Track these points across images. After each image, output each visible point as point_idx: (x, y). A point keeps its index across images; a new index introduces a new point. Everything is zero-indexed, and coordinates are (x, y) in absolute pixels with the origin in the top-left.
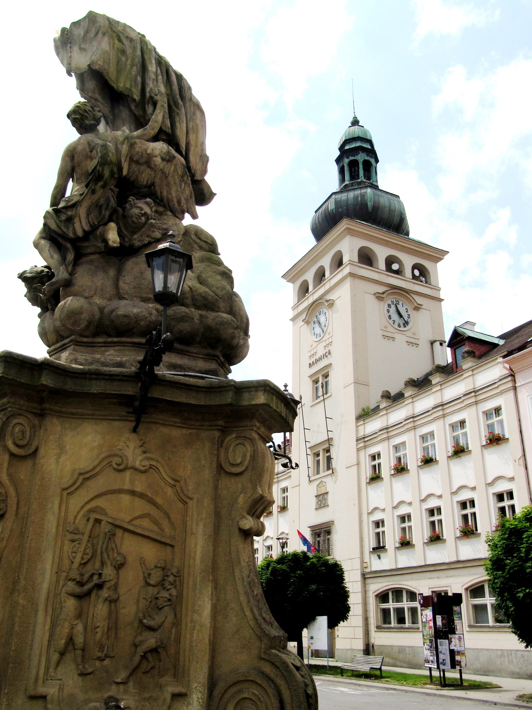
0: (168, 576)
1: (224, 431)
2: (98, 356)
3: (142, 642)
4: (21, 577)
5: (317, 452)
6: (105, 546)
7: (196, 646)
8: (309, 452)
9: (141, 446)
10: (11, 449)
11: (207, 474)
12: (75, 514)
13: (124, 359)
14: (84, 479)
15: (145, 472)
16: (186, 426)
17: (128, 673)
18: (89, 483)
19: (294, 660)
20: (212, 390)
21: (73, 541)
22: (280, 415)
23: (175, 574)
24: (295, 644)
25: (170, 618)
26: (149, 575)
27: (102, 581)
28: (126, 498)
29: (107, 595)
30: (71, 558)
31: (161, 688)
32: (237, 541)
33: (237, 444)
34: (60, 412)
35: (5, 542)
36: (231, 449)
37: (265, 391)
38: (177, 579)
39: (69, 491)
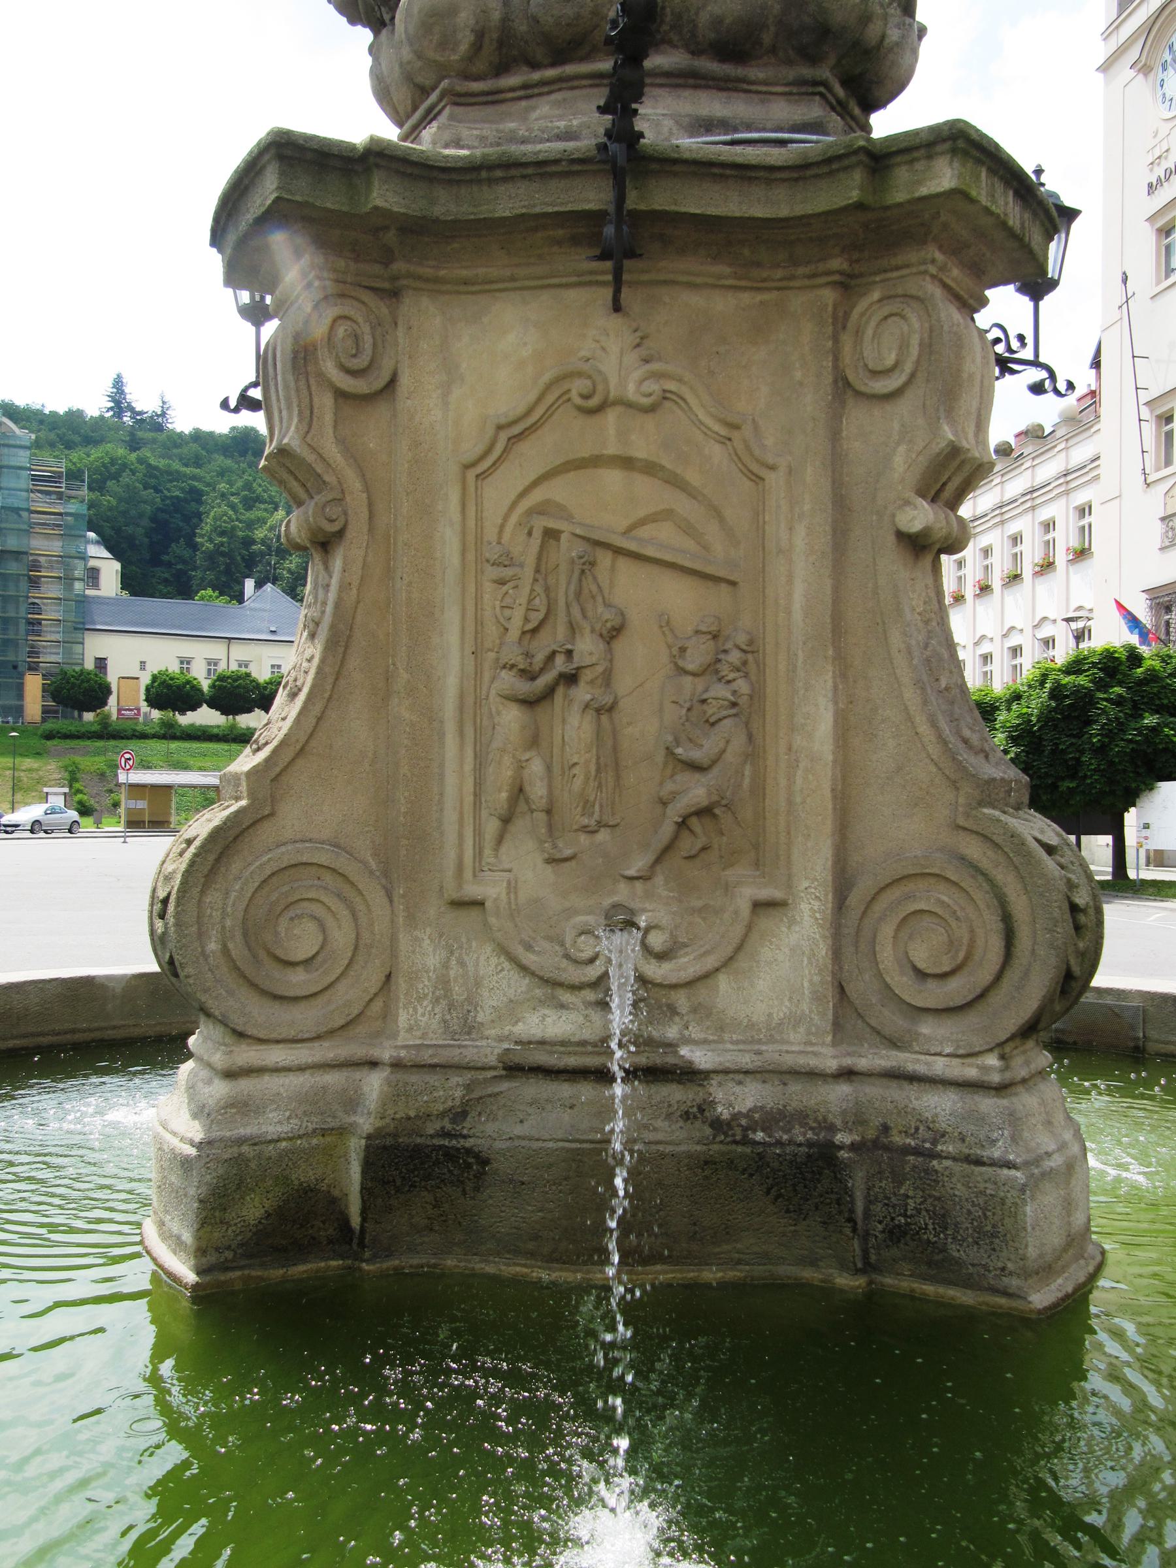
0: (725, 651)
1: (849, 285)
2: (512, 125)
3: (674, 795)
4: (399, 664)
5: (1166, 412)
6: (572, 588)
7: (804, 802)
8: (1145, 413)
9: (638, 345)
10: (334, 379)
11: (812, 402)
12: (500, 521)
13: (575, 123)
14: (509, 439)
15: (652, 409)
16: (749, 284)
17: (650, 857)
18: (524, 447)
19: (1042, 832)
20: (809, 173)
21: (502, 582)
22: (1004, 225)
23: (745, 647)
24: (1108, 839)
25: (738, 742)
26: (683, 650)
27: (575, 666)
28: (613, 478)
29: (589, 697)
30: (502, 620)
31: (727, 889)
32: (892, 563)
33: (886, 318)
34: (437, 280)
35: (355, 591)
36: (870, 332)
37: (954, 151)
38: (750, 657)
39: (477, 471)
